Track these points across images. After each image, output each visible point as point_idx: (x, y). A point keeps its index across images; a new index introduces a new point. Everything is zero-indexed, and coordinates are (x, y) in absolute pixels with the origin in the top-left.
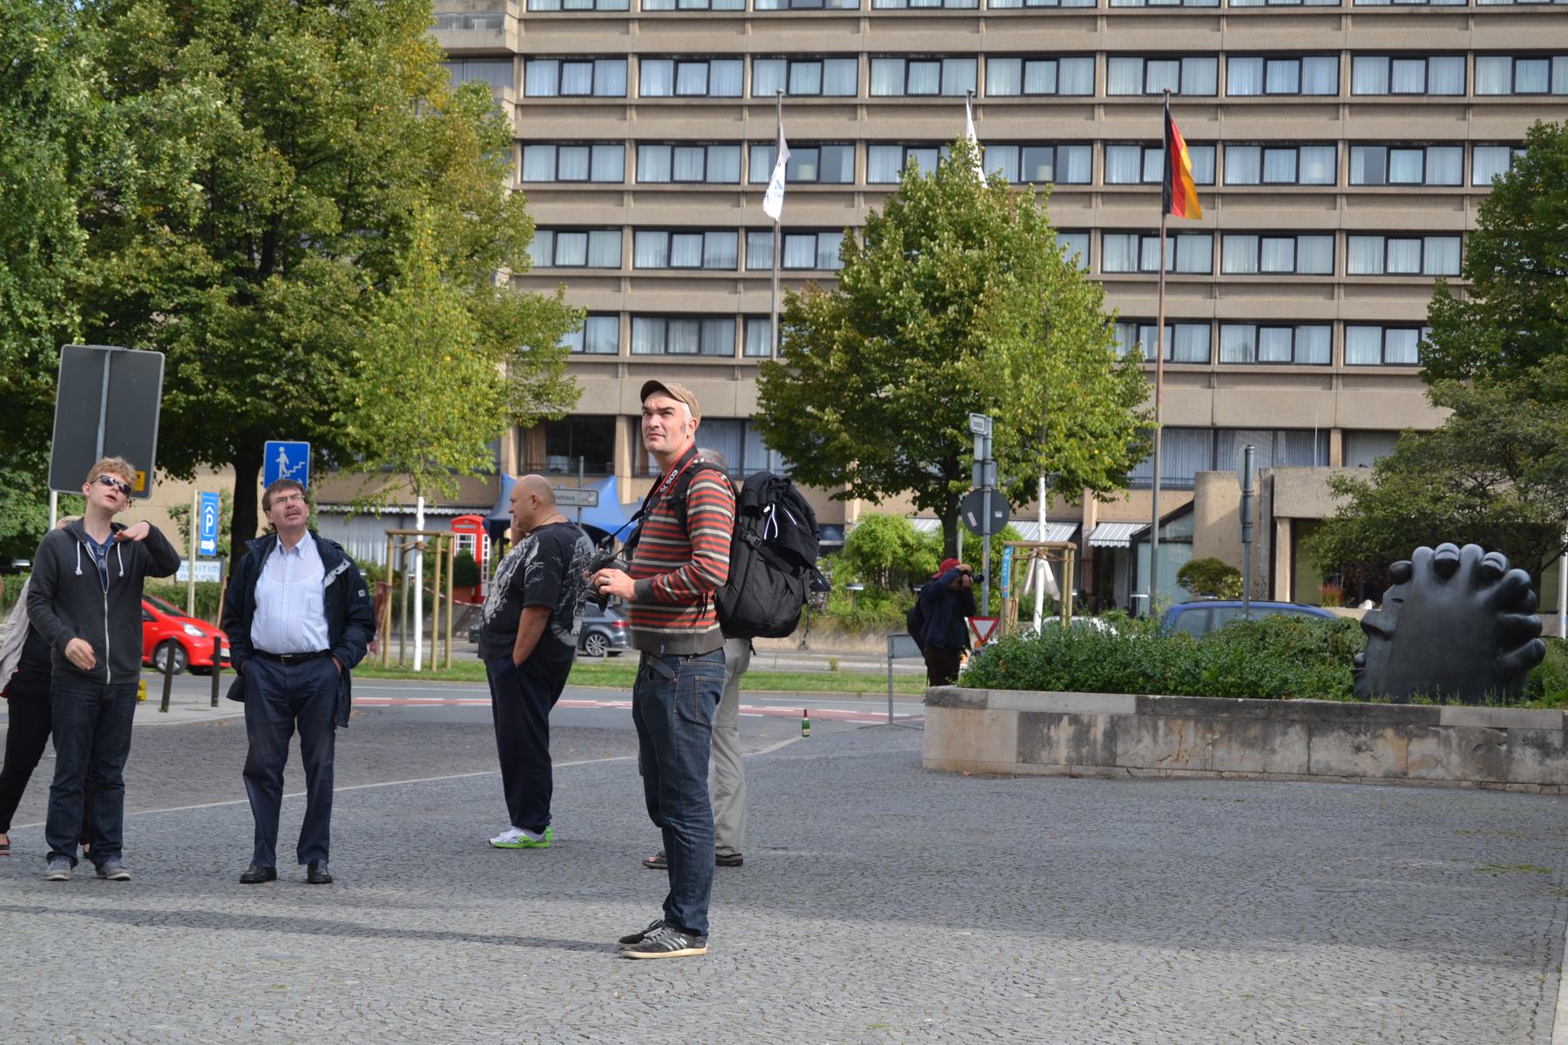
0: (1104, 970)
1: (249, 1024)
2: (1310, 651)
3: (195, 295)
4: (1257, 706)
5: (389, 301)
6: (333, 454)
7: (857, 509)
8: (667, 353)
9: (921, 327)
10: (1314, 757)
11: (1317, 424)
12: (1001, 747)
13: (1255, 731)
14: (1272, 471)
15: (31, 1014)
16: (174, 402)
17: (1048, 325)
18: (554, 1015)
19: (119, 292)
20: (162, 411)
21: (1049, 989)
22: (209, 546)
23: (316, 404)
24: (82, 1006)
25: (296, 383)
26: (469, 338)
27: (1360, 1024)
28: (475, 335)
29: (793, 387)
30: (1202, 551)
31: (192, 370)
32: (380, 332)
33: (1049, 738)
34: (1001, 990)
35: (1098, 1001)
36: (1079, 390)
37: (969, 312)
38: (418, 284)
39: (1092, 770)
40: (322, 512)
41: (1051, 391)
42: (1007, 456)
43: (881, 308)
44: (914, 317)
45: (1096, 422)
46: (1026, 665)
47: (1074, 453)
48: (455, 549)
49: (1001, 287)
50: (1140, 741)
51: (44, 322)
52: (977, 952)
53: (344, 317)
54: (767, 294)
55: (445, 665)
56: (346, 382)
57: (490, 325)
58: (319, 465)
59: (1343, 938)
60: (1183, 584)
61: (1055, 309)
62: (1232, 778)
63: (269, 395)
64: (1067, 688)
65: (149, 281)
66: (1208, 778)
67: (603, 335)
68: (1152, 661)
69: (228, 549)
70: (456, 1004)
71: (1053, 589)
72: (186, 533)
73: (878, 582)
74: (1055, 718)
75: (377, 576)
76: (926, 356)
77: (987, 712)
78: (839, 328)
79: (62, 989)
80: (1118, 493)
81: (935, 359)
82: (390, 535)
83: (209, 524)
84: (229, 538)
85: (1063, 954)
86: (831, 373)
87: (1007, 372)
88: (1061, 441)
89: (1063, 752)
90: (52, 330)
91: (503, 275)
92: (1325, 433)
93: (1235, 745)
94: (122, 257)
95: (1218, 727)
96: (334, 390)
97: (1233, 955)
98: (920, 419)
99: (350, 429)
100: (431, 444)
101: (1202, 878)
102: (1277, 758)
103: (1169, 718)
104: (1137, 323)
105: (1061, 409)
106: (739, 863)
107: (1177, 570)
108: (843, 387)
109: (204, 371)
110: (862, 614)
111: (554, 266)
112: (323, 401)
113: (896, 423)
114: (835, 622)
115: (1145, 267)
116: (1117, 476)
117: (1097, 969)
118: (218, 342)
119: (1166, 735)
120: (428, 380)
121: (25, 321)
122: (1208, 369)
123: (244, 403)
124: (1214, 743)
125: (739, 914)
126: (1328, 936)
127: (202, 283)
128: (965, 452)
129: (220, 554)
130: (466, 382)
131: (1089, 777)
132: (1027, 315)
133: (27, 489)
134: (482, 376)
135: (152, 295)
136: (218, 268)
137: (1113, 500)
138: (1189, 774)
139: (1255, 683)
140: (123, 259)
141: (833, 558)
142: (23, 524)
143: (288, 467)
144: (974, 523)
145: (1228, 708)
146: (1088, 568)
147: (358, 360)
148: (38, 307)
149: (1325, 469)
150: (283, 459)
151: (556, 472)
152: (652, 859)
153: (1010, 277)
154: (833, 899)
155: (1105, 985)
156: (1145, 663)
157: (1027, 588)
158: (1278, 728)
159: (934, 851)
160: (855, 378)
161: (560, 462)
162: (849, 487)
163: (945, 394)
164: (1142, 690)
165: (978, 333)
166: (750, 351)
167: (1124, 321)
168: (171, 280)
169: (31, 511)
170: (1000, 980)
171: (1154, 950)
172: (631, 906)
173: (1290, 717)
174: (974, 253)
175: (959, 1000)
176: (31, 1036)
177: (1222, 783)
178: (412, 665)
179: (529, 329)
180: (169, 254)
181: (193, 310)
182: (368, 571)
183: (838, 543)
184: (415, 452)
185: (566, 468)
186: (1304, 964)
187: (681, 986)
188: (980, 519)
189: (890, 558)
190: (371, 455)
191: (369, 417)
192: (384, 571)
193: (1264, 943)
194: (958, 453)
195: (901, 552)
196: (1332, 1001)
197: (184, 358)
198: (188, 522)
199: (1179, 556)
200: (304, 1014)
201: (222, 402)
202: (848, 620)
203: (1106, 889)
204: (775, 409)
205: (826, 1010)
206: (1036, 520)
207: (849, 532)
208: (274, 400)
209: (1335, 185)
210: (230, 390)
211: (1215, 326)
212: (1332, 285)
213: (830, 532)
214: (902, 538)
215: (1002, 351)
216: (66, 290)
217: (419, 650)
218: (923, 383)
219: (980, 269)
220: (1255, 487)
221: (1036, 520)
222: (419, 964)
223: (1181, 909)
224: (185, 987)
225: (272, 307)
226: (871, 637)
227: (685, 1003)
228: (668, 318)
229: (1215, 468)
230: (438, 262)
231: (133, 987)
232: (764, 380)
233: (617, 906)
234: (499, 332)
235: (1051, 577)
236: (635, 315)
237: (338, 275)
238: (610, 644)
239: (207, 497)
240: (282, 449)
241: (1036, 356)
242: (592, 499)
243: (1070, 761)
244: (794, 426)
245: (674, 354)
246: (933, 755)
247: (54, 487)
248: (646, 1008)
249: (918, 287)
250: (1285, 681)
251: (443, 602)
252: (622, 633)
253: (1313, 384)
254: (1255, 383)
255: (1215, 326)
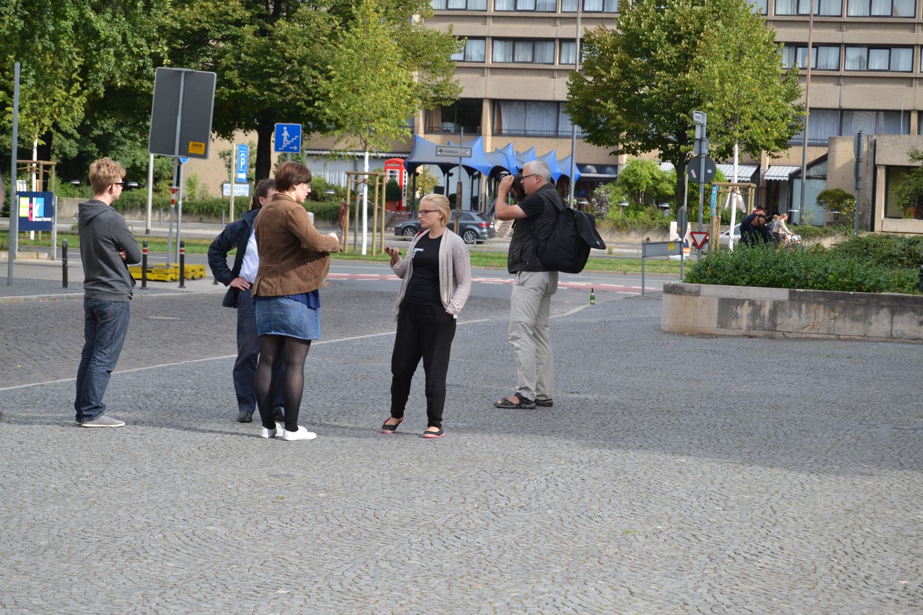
0: (763, 489)
1: (262, 527)
2: (895, 256)
3: (234, 30)
4: (861, 297)
5: (348, 35)
6: (317, 125)
7: (625, 158)
8: (514, 61)
9: (666, 53)
10: (896, 327)
11: (903, 107)
12: (708, 319)
13: (859, 312)
14: (875, 137)
15: (138, 517)
16: (222, 94)
17: (741, 53)
18: (439, 522)
19: (188, 29)
20: (216, 99)
21: (730, 504)
22: (243, 176)
23: (305, 96)
24: (166, 511)
25: (293, 83)
26: (396, 57)
27: (914, 533)
28: (399, 56)
29: (588, 88)
30: (831, 185)
31: (233, 75)
32: (343, 53)
33: (737, 314)
34: (702, 504)
35: (759, 514)
36: (759, 92)
37: (695, 44)
38: (366, 24)
39: (762, 333)
40: (309, 155)
41: (742, 93)
42: (716, 130)
43: (642, 41)
44: (662, 46)
45: (770, 111)
46: (724, 270)
47: (757, 131)
48: (387, 179)
49: (715, 29)
50: (791, 316)
51: (146, 51)
52: (689, 475)
53: (323, 44)
54: (574, 27)
55: (380, 252)
56: (324, 83)
57: (408, 49)
58: (307, 130)
59: (907, 465)
60: (820, 204)
61: (746, 43)
62: (845, 340)
63: (278, 90)
64: (748, 284)
65: (208, 22)
66: (831, 339)
67: (475, 50)
68: (799, 269)
69: (254, 177)
70: (383, 512)
71: (742, 206)
72: (229, 167)
73: (637, 201)
74: (741, 302)
75: (340, 194)
76: (668, 69)
77: (700, 298)
78: (616, 53)
79: (155, 497)
80: (782, 153)
81: (674, 72)
82: (349, 174)
83: (242, 164)
84: (254, 170)
85: (739, 477)
86: (611, 80)
87: (717, 81)
88: (748, 122)
89: (744, 322)
90: (151, 55)
91: (416, 18)
92: (908, 113)
93: (847, 320)
94: (192, 8)
95: (838, 309)
96: (316, 88)
97: (841, 478)
98: (664, 108)
99: (327, 111)
100: (373, 121)
101: (825, 417)
102: (873, 328)
103: (809, 303)
104: (795, 46)
105: (748, 103)
106: (550, 405)
107: (817, 195)
108: (619, 88)
109: (240, 76)
110: (628, 220)
111: (447, 9)
112: (309, 93)
113: (651, 110)
114: (611, 224)
115: (801, 12)
116: (782, 143)
117: (760, 489)
118: (248, 59)
119: (807, 313)
120: (372, 83)
121: (135, 50)
122: (838, 74)
123: (263, 95)
124: (835, 318)
125: (549, 442)
126: (897, 464)
127: (239, 23)
128: (690, 128)
129: (249, 180)
130: (394, 84)
131: (760, 337)
132: (729, 46)
133: (136, 139)
134: (404, 80)
135: (209, 30)
136: (248, 14)
137: (779, 157)
138: (820, 336)
139: (860, 283)
140: (192, 9)
141: (610, 186)
142: (134, 160)
143: (289, 139)
144: (695, 176)
145: (844, 297)
146: (763, 193)
147: (331, 70)
148: (143, 42)
149: (907, 136)
150: (286, 134)
151: (447, 132)
152: (499, 402)
153: (719, 24)
154: (605, 432)
155: (764, 501)
156: (795, 270)
157: (726, 206)
158: (874, 310)
159: (666, 395)
160: (625, 83)
161: (450, 126)
162: (621, 147)
163: (679, 93)
164: (793, 286)
165: (700, 57)
166: (564, 61)
167: (788, 44)
168: (221, 22)
169: (139, 153)
170: (702, 497)
171: (794, 474)
172: (486, 436)
173: (881, 304)
174: (698, 9)
175: (678, 511)
176: (138, 534)
177: (839, 343)
178: (361, 251)
179: (431, 51)
180: (219, 6)
181: (234, 39)
182: (336, 190)
183: (614, 176)
184: (364, 125)
185: (453, 130)
186: (883, 485)
187: (514, 500)
188: (698, 173)
189: (645, 186)
190: (339, 127)
191: (337, 104)
192: (345, 191)
193: (859, 469)
194: (686, 128)
195: (651, 182)
196: (898, 515)
197: (228, 68)
198: (230, 161)
199: (819, 187)
200: (294, 519)
201: (250, 94)
202: (619, 224)
203: (767, 426)
204: (577, 100)
205: (599, 519)
206: (732, 163)
207: (621, 169)
208: (281, 94)
209: (912, 72)
210: (255, 87)
211: (843, 48)
212: (914, 24)
213: (609, 169)
214: (652, 175)
215: (714, 68)
216: (158, 31)
217: (365, 237)
218: (666, 86)
219: (701, 18)
220: (865, 147)
221: (732, 163)
222: (362, 481)
223: (811, 443)
224: (226, 497)
225: (279, 38)
226: (633, 234)
227: (516, 513)
228: (515, 40)
229: (841, 134)
230: (378, 12)
231: (196, 496)
232: (571, 83)
233: (478, 436)
234: (415, 52)
235: (740, 198)
236: (494, 39)
237: (319, 19)
238: (478, 236)
239: (241, 146)
240: (285, 128)
241: (733, 72)
242: (468, 153)
243: (749, 328)
244: (589, 111)
245: (518, 62)
246: (667, 322)
247: (152, 151)
248: (493, 516)
249: (664, 28)
250: (879, 281)
251: (380, 210)
252: (485, 230)
253: (900, 83)
254: (867, 83)
255: (843, 48)
